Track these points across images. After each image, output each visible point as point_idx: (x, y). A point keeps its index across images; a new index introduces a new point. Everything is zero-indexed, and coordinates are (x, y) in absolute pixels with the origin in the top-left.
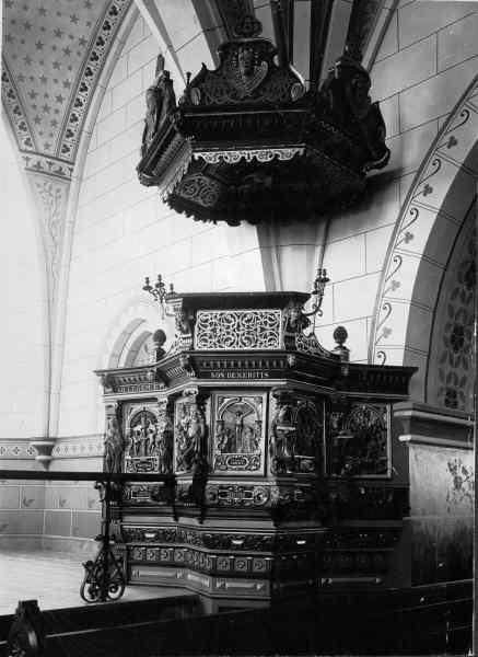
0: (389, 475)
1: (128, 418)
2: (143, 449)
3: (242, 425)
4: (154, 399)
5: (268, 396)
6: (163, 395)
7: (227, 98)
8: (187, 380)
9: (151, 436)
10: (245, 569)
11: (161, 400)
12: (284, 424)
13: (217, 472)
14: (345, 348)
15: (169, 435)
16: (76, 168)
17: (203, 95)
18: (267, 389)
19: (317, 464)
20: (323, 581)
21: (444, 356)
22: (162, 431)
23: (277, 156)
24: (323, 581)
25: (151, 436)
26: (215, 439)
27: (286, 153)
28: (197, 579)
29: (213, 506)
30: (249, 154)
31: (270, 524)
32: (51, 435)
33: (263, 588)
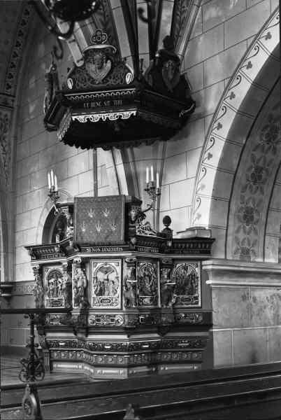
0: (200, 304)
1: (46, 274)
2: (55, 293)
3: (108, 280)
4: (59, 263)
5: (122, 261)
6: (65, 261)
7: (89, 83)
8: (76, 253)
9: (59, 285)
10: (113, 362)
11: (64, 264)
12: (131, 278)
13: (95, 307)
14: (170, 229)
15: (69, 285)
16: (16, 99)
17: (75, 82)
18: (122, 258)
19: (154, 301)
20: (162, 368)
21: (239, 228)
22: (65, 282)
23: (121, 116)
24: (162, 368)
25: (59, 285)
26: (93, 288)
27: (126, 115)
28: (88, 368)
29: (94, 327)
30: (104, 116)
31: (125, 337)
32: (10, 280)
33: (124, 373)
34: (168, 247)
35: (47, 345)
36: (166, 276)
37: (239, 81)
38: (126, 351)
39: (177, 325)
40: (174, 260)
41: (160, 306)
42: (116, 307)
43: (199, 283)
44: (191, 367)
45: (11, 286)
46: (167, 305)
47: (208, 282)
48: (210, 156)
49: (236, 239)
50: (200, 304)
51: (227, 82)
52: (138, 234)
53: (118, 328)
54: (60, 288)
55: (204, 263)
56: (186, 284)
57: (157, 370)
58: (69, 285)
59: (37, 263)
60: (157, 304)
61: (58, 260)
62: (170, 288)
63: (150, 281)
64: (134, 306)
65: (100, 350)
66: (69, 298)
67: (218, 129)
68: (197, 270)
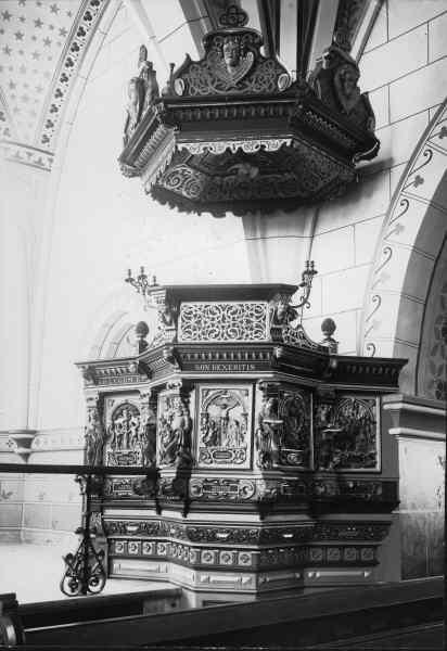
0: (378, 468)
1: (109, 411)
2: (125, 442)
3: (227, 419)
4: (136, 392)
5: (254, 387)
9: (133, 429)
12: (270, 416)
13: (202, 465)
15: (152, 429)
17: (187, 85)
18: (253, 381)
19: (305, 458)
20: (310, 575)
23: (263, 146)
24: (310, 575)
25: (133, 429)
27: (273, 145)
29: (198, 499)
33: (250, 581)
34: (331, 369)
35: (107, 530)
36: (323, 418)
37: (388, 256)
38: (253, 544)
39: (337, 504)
40: (339, 392)
41: (312, 468)
42: (242, 466)
43: (378, 431)
44: (359, 573)
45: (30, 436)
46: (326, 466)
47: (392, 431)
48: (419, 181)
49: (432, 365)
50: (378, 468)
51: (434, 112)
52: (286, 342)
53: (243, 501)
54: (134, 434)
55: (385, 399)
56: (357, 433)
57: (302, 577)
58: (152, 429)
59: (94, 392)
60: (308, 465)
61: (132, 387)
62: (331, 438)
63: (298, 423)
64: (275, 465)
65: (209, 541)
66: (150, 452)
67: (441, 137)
68: (376, 410)
